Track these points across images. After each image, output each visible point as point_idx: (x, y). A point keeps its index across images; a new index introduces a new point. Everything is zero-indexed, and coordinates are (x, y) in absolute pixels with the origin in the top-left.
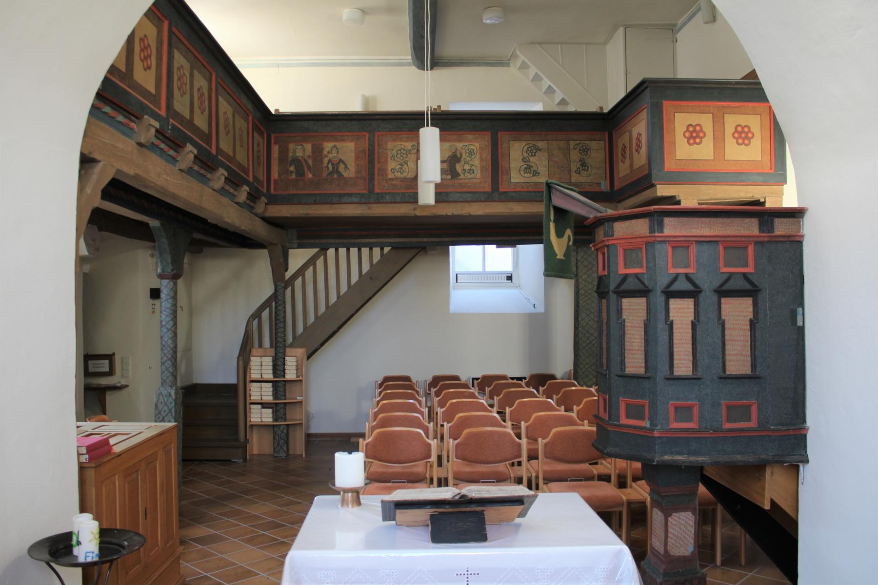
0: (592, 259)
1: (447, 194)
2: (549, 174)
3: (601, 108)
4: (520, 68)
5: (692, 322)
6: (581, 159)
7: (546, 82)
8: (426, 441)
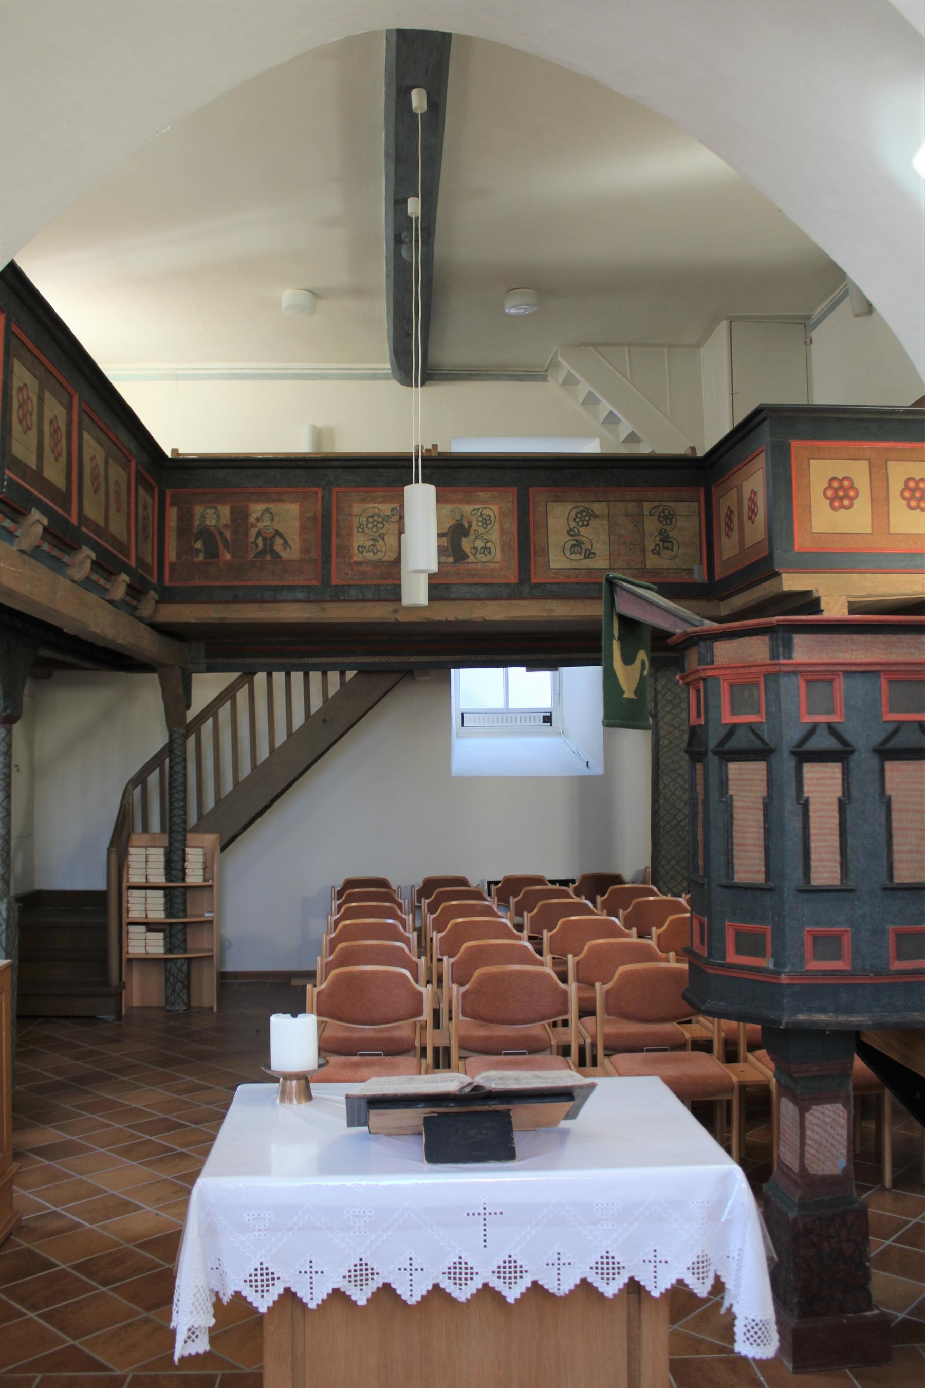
0: (679, 690)
1: (448, 586)
2: (610, 554)
3: (693, 449)
4: (563, 384)
5: (840, 800)
6: (661, 530)
7: (606, 407)
8: (414, 988)
